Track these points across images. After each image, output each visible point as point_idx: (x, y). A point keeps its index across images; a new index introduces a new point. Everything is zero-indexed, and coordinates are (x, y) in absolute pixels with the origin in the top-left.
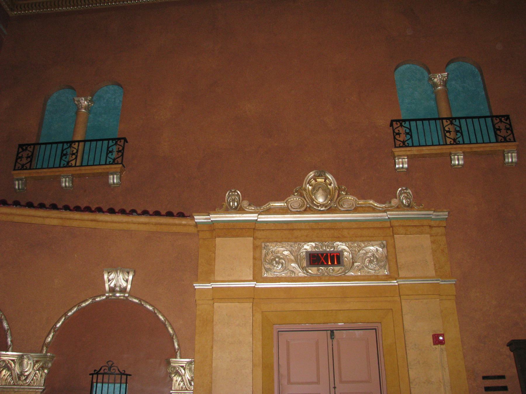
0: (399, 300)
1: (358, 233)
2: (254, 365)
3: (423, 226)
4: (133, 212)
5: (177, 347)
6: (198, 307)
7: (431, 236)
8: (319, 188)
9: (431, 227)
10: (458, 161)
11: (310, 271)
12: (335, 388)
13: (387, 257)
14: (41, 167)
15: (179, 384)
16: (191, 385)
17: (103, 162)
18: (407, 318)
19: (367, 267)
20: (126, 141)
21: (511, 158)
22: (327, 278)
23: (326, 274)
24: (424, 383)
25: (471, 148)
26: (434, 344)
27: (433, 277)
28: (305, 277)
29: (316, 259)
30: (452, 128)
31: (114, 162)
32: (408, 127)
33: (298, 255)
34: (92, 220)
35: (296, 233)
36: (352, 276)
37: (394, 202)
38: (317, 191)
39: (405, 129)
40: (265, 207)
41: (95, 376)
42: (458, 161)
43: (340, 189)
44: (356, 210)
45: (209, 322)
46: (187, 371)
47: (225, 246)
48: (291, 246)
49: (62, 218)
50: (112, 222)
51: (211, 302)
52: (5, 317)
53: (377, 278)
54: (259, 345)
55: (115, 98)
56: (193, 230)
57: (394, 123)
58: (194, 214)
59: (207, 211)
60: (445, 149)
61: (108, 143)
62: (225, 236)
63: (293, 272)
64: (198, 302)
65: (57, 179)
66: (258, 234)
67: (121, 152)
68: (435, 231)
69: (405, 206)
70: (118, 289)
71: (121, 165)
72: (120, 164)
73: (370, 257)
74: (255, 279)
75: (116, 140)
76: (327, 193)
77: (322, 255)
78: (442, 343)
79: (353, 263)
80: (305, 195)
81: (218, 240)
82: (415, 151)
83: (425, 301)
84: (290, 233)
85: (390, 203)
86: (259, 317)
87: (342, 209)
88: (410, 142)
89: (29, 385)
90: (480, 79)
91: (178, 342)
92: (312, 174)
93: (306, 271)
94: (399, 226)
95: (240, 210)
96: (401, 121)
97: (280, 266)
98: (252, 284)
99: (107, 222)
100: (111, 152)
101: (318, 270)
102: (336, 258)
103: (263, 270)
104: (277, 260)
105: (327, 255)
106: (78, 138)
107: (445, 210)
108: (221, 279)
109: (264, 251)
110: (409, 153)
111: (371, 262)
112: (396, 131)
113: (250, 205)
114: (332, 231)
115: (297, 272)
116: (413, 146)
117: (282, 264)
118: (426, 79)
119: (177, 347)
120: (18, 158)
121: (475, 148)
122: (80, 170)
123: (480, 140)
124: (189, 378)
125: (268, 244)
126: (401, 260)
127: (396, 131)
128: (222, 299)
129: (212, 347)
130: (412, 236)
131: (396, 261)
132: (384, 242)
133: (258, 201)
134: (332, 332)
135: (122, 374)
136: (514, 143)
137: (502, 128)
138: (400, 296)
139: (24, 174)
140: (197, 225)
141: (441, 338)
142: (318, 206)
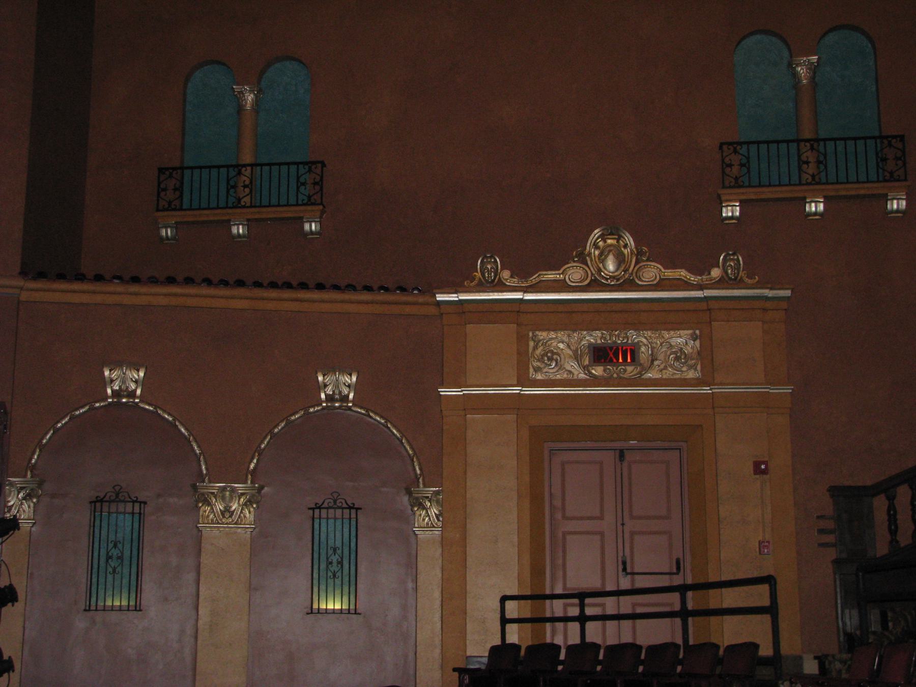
2: (520, 497)
3: (753, 309)
4: (351, 287)
5: (418, 472)
6: (445, 420)
8: (610, 251)
9: (765, 310)
11: (593, 372)
13: (699, 353)
15: (424, 520)
16: (438, 520)
17: (292, 200)
19: (671, 366)
20: (323, 165)
23: (615, 375)
26: (755, 474)
27: (761, 384)
28: (586, 380)
29: (601, 354)
32: (746, 154)
34: (296, 300)
36: (650, 379)
37: (716, 273)
38: (606, 257)
40: (534, 279)
41: (317, 511)
42: (815, 207)
43: (640, 253)
44: (660, 285)
47: (480, 336)
48: (569, 336)
50: (323, 301)
51: (462, 413)
52: (194, 438)
53: (685, 383)
56: (433, 310)
57: (725, 147)
58: (435, 291)
63: (570, 372)
64: (444, 412)
67: (319, 183)
69: (730, 279)
70: (337, 397)
71: (321, 207)
72: (318, 204)
76: (621, 260)
77: (611, 348)
78: (764, 472)
79: (653, 361)
80: (589, 262)
81: (469, 327)
82: (751, 194)
85: (709, 274)
89: (236, 523)
91: (420, 465)
93: (589, 371)
94: (720, 309)
95: (501, 286)
96: (734, 146)
97: (554, 364)
98: (516, 390)
99: (314, 301)
101: (604, 371)
103: (531, 370)
106: (247, 158)
107: (788, 286)
111: (677, 359)
112: (727, 160)
113: (512, 277)
115: (576, 373)
119: (418, 472)
120: (160, 190)
121: (843, 190)
124: (437, 512)
127: (727, 160)
128: (475, 410)
129: (465, 473)
130: (736, 323)
131: (712, 360)
133: (524, 270)
135: (350, 508)
138: (713, 408)
142: (607, 279)
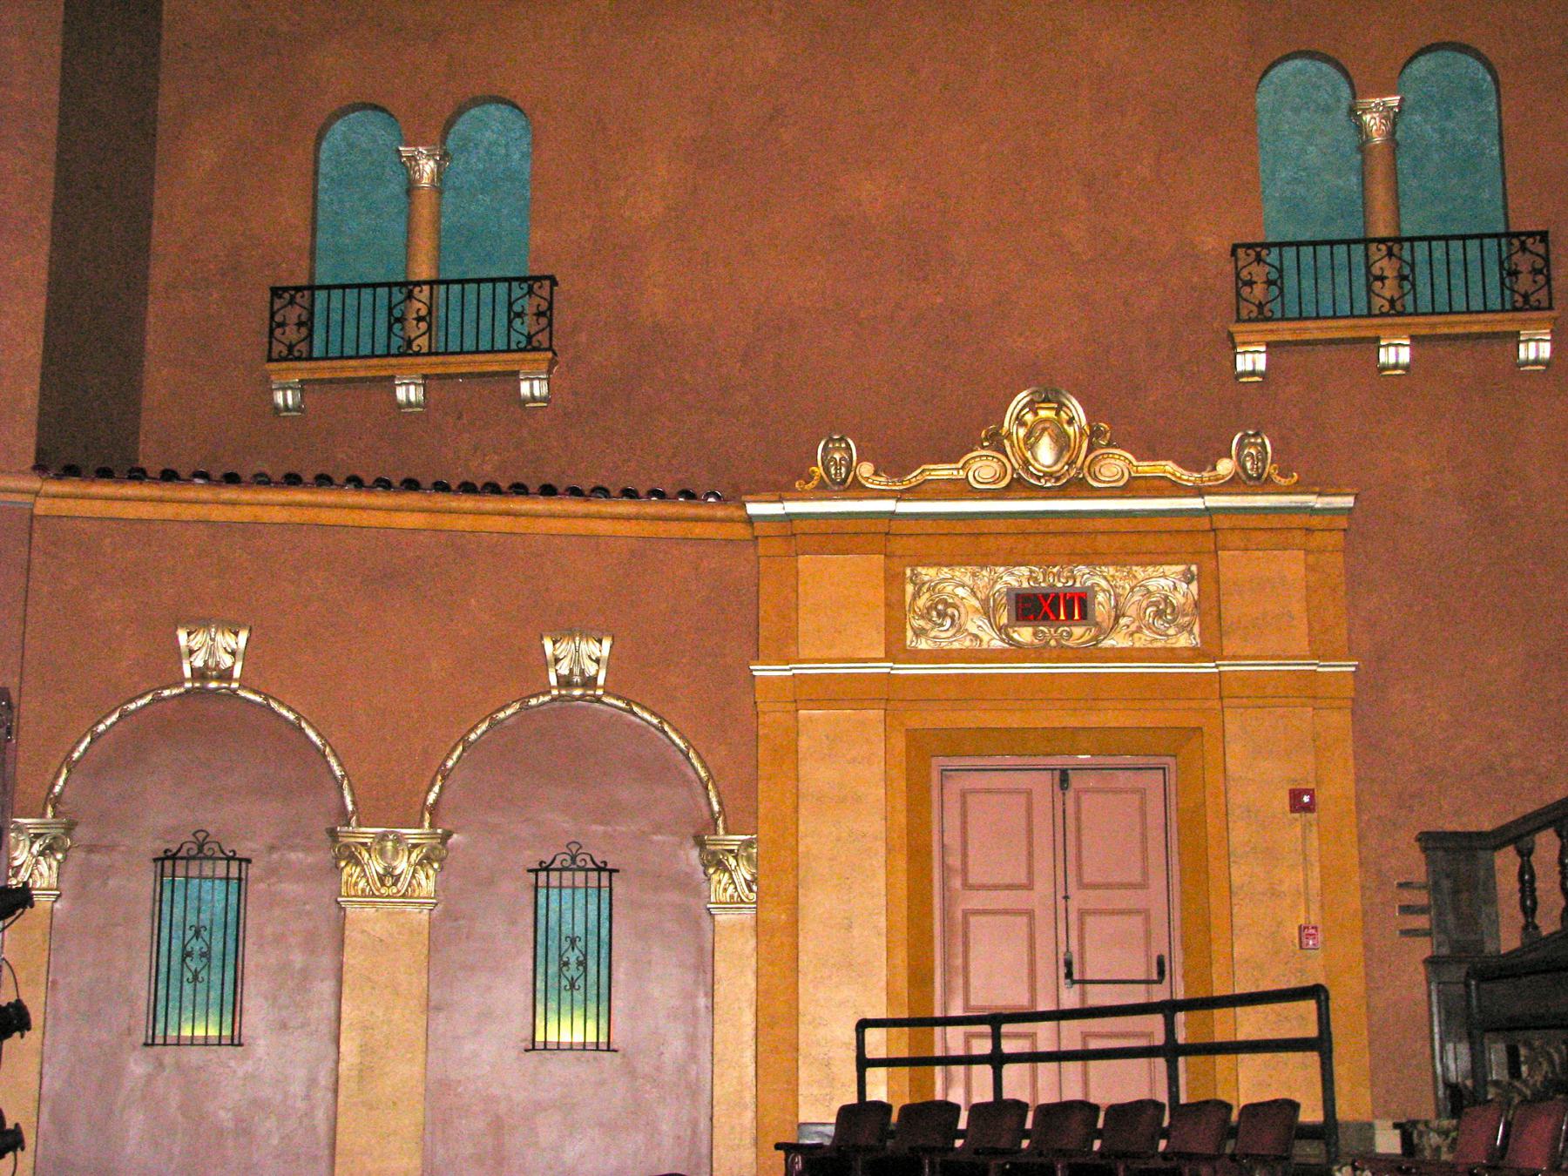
0: (1218, 707)
1: (1137, 541)
2: (889, 851)
3: (1289, 529)
4: (601, 492)
7: (1308, 552)
8: (1044, 430)
10: (1396, 354)
11: (1015, 636)
12: (1066, 898)
14: (338, 354)
16: (751, 890)
18: (1234, 748)
21: (1536, 349)
22: (1054, 654)
23: (1053, 643)
24: (1264, 894)
25: (1433, 326)
27: (1303, 658)
28: (1003, 651)
30: (1389, 265)
31: (530, 346)
33: (987, 599)
34: (508, 513)
35: (990, 544)
36: (1113, 649)
37: (1225, 467)
38: (1038, 439)
39: (1268, 269)
40: (914, 478)
42: (1396, 354)
43: (1095, 433)
44: (1131, 488)
45: (789, 753)
46: (743, 862)
48: (974, 575)
49: (431, 511)
50: (552, 516)
51: (791, 707)
54: (901, 805)
55: (507, 145)
56: (740, 531)
59: (781, 492)
60: (1364, 328)
61: (510, 289)
62: (821, 551)
64: (760, 706)
65: (388, 383)
66: (896, 545)
68: (1319, 539)
69: (1250, 477)
70: (577, 679)
71: (550, 355)
72: (546, 350)
73: (1156, 604)
74: (889, 657)
75: (530, 281)
76: (1062, 444)
77: (1045, 596)
78: (1308, 808)
79: (1117, 618)
80: (1008, 449)
82: (1285, 332)
83: (1279, 711)
84: (972, 542)
86: (899, 743)
87: (1095, 484)
88: (1276, 306)
90: (1492, 108)
92: (1023, 397)
93: (1007, 635)
95: (855, 489)
96: (1258, 249)
100: (519, 315)
101: (1035, 634)
102: (1077, 604)
103: (909, 634)
104: (940, 607)
105: (1057, 596)
106: (423, 271)
107: (1348, 490)
108: (814, 655)
109: (910, 588)
110: (1271, 338)
114: (1072, 540)
115: (986, 638)
116: (1283, 319)
117: (952, 617)
118: (1344, 106)
120: (274, 325)
122: (443, 364)
123: (1460, 304)
125: (919, 569)
126: (1231, 612)
127: (1244, 274)
128: (815, 702)
130: (1260, 554)
132: (1194, 568)
134: (1064, 778)
136: (1547, 314)
137: (1520, 268)
138: (1221, 698)
139: (303, 370)
140: (750, 520)
141: (1306, 799)
142: (1039, 478)
